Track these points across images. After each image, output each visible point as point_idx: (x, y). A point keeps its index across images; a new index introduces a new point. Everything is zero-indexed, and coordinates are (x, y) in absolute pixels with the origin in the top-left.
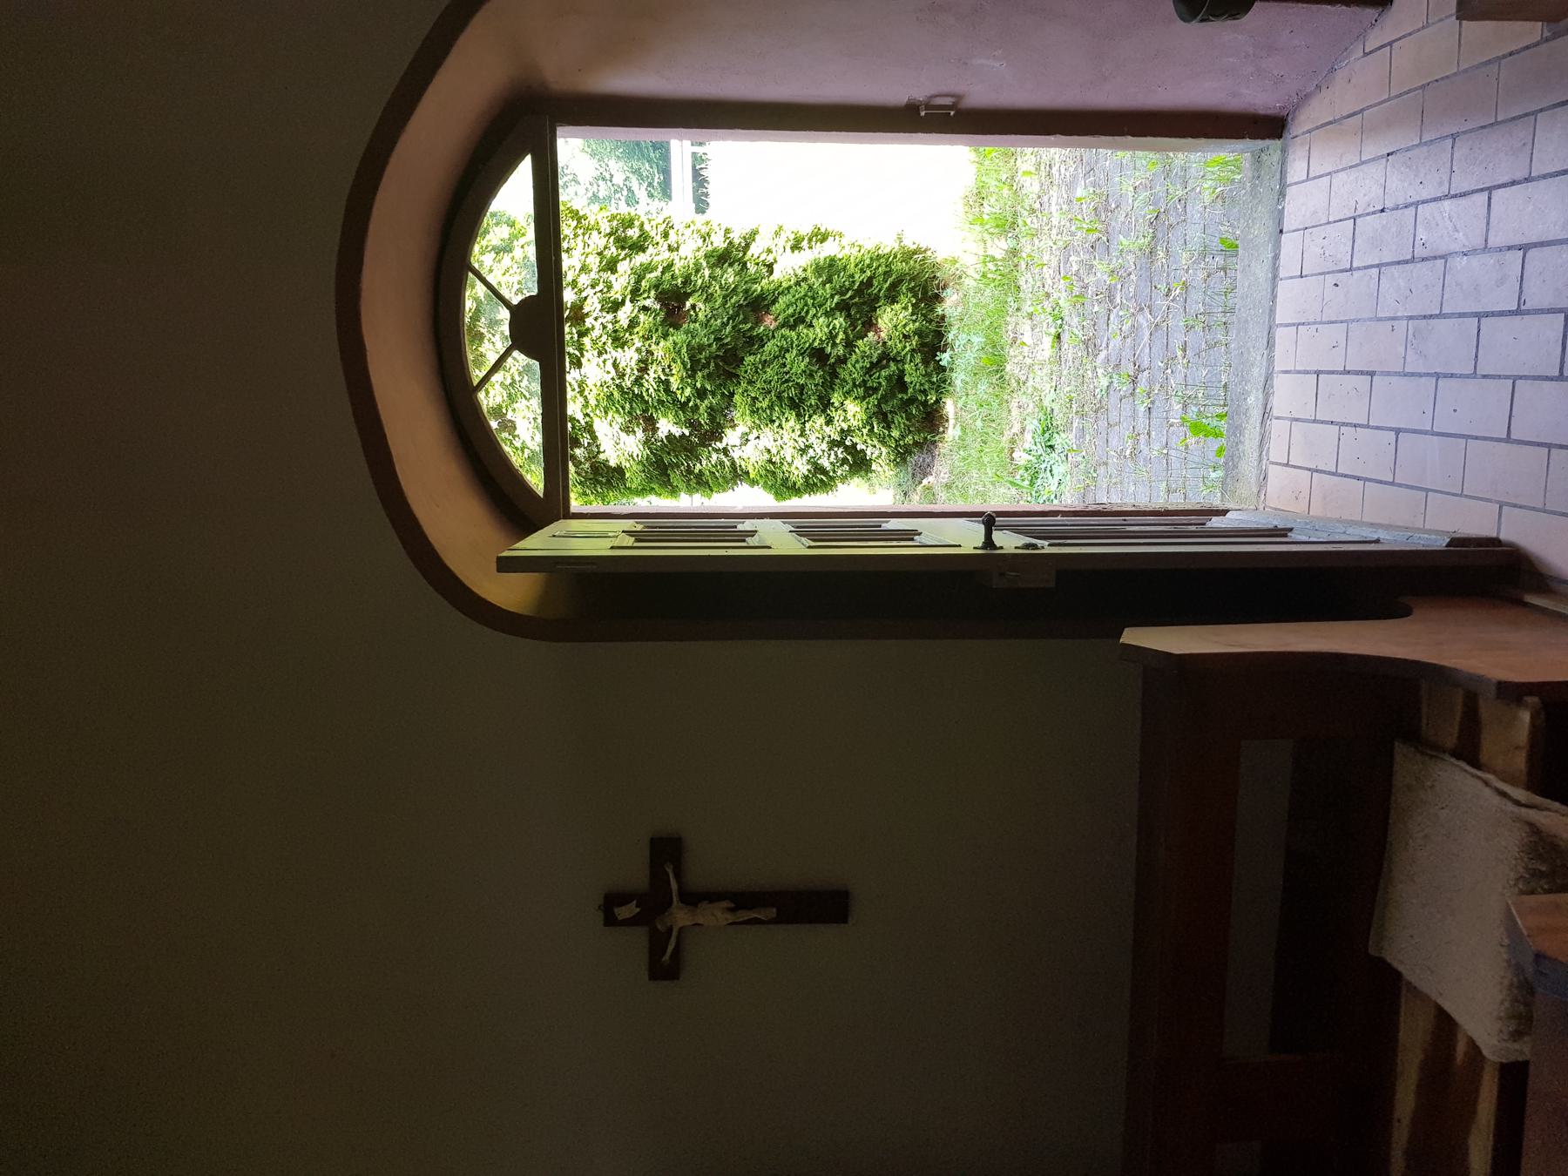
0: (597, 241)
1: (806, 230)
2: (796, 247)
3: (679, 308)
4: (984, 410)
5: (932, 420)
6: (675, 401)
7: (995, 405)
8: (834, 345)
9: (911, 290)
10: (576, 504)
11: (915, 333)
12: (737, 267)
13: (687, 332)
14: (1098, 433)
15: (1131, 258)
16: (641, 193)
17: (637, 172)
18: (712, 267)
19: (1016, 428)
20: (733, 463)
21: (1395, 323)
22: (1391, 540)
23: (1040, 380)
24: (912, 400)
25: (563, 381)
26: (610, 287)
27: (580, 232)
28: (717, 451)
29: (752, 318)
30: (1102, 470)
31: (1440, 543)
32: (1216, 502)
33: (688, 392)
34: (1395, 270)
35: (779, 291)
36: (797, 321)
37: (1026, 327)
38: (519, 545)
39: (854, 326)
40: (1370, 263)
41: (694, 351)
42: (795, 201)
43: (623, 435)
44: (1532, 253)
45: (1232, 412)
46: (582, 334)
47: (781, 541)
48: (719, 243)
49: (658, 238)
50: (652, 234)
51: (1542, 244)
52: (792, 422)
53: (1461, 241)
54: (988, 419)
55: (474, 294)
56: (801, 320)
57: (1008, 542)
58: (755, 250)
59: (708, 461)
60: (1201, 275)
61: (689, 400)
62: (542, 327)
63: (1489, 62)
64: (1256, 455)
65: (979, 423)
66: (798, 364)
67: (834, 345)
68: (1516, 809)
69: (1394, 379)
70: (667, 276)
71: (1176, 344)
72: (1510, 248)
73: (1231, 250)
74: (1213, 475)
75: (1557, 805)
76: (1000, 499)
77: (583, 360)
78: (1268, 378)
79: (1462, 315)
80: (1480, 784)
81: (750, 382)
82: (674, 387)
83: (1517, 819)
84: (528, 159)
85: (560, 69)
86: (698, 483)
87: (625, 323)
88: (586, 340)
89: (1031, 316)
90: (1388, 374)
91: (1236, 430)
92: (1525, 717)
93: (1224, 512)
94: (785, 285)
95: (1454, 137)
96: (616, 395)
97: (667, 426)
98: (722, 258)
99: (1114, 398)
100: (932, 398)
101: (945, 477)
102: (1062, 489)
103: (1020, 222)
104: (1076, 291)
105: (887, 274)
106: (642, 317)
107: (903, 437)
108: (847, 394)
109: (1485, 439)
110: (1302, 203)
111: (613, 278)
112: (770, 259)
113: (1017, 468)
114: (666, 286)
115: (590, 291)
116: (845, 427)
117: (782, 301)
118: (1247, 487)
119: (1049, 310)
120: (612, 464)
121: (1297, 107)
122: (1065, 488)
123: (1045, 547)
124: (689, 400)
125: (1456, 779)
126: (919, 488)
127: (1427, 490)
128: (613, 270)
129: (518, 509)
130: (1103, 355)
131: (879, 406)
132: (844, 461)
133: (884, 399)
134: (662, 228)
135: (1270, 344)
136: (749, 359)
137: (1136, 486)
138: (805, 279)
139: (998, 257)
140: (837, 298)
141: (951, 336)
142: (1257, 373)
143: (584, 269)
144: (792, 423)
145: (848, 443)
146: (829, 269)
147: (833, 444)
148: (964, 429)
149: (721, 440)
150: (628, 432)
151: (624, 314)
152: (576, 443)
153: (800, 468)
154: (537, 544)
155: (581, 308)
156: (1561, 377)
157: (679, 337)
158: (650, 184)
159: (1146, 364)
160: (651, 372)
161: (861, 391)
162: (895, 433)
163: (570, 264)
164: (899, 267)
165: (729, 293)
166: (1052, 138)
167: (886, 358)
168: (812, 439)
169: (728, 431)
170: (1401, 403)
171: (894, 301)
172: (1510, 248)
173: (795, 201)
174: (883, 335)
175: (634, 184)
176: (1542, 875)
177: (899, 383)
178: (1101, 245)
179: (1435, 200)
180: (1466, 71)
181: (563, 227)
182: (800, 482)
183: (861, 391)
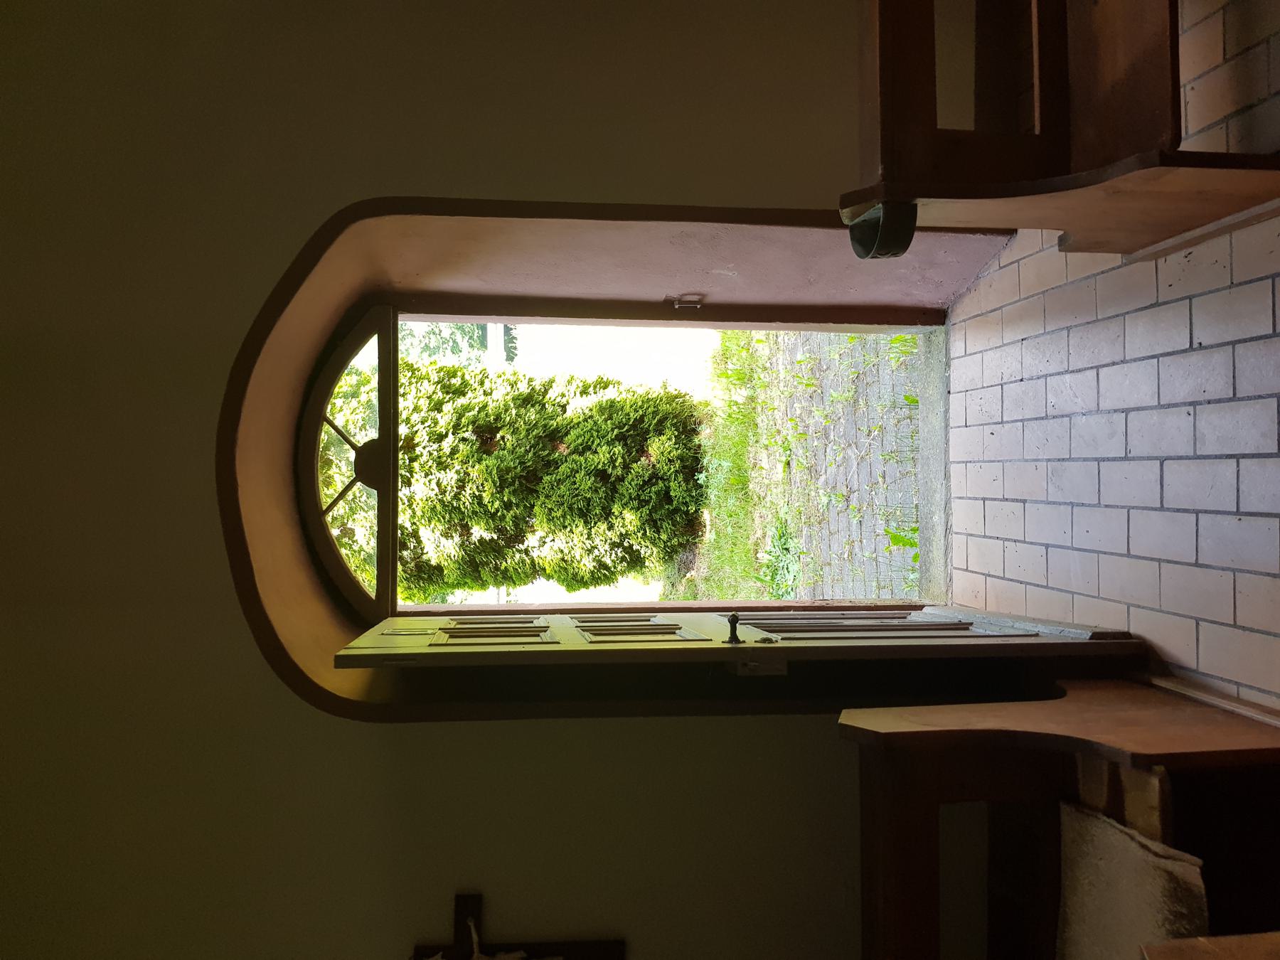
0: (427, 388)
1: (591, 379)
2: (584, 392)
4: (734, 519)
5: (692, 526)
6: (486, 512)
7: (742, 516)
8: (614, 467)
10: (403, 603)
13: (497, 458)
15: (840, 406)
16: (463, 344)
17: (461, 329)
19: (759, 534)
20: (533, 561)
21: (1038, 464)
22: (1049, 634)
23: (776, 496)
24: (676, 510)
25: (396, 497)
26: (436, 424)
27: (414, 380)
28: (519, 551)
30: (827, 569)
31: (1085, 636)
32: (915, 599)
33: (497, 504)
34: (1032, 423)
35: (571, 426)
36: (585, 449)
37: (763, 455)
38: (355, 643)
40: (1016, 418)
41: (503, 473)
42: (582, 364)
43: (443, 540)
44: (1132, 415)
45: (922, 526)
46: (412, 460)
47: (568, 637)
48: (524, 389)
49: (476, 386)
50: (471, 382)
51: (1138, 409)
52: (580, 528)
53: (1079, 405)
54: (737, 526)
55: (326, 434)
56: (589, 448)
57: (750, 636)
58: (552, 394)
59: (512, 560)
60: (893, 422)
62: (380, 465)
63: (1088, 277)
64: (942, 561)
65: (729, 529)
67: (614, 467)
68: (1156, 860)
69: (1040, 506)
70: (482, 414)
71: (878, 472)
72: (1115, 411)
73: (913, 404)
74: (912, 576)
75: (1188, 856)
76: (747, 594)
77: (413, 480)
78: (947, 503)
79: (1085, 460)
80: (1128, 839)
81: (547, 497)
83: (1157, 868)
84: (373, 595)
85: (404, 271)
87: (447, 451)
88: (416, 465)
89: (766, 447)
90: (1036, 502)
91: (927, 541)
92: (1155, 782)
93: (920, 608)
95: (1069, 329)
97: (479, 532)
98: (526, 401)
99: (833, 514)
100: (692, 509)
102: (797, 587)
103: (755, 376)
104: (800, 429)
105: (655, 413)
106: (461, 446)
107: (670, 539)
108: (624, 506)
109: (1112, 554)
110: (962, 373)
111: (439, 416)
112: (564, 401)
113: (761, 567)
114: (481, 422)
115: (420, 426)
116: (623, 531)
117: (573, 433)
118: (938, 587)
119: (780, 443)
120: (433, 563)
121: (955, 303)
122: (798, 583)
123: (779, 641)
124: (497, 511)
125: (1107, 833)
126: (684, 581)
127: (1073, 593)
128: (440, 411)
129: (358, 611)
130: (823, 479)
132: (623, 559)
135: (947, 476)
136: (547, 478)
137: (853, 586)
138: (591, 417)
139: (741, 401)
140: (616, 431)
141: (705, 461)
142: (939, 497)
144: (581, 528)
145: (626, 544)
146: (610, 409)
147: (614, 545)
148: (718, 534)
151: (447, 444)
152: (404, 546)
153: (587, 565)
154: (368, 642)
155: (413, 439)
156: (1275, 334)
157: (490, 461)
158: (471, 338)
159: (855, 487)
160: (467, 489)
161: (636, 503)
162: (664, 537)
163: (404, 405)
164: (664, 407)
165: (531, 427)
167: (655, 477)
168: (597, 541)
169: (529, 535)
172: (1115, 411)
173: (582, 364)
175: (458, 337)
176: (1182, 915)
177: (666, 497)
178: (818, 395)
179: (1059, 374)
180: (1072, 282)
181: (401, 376)
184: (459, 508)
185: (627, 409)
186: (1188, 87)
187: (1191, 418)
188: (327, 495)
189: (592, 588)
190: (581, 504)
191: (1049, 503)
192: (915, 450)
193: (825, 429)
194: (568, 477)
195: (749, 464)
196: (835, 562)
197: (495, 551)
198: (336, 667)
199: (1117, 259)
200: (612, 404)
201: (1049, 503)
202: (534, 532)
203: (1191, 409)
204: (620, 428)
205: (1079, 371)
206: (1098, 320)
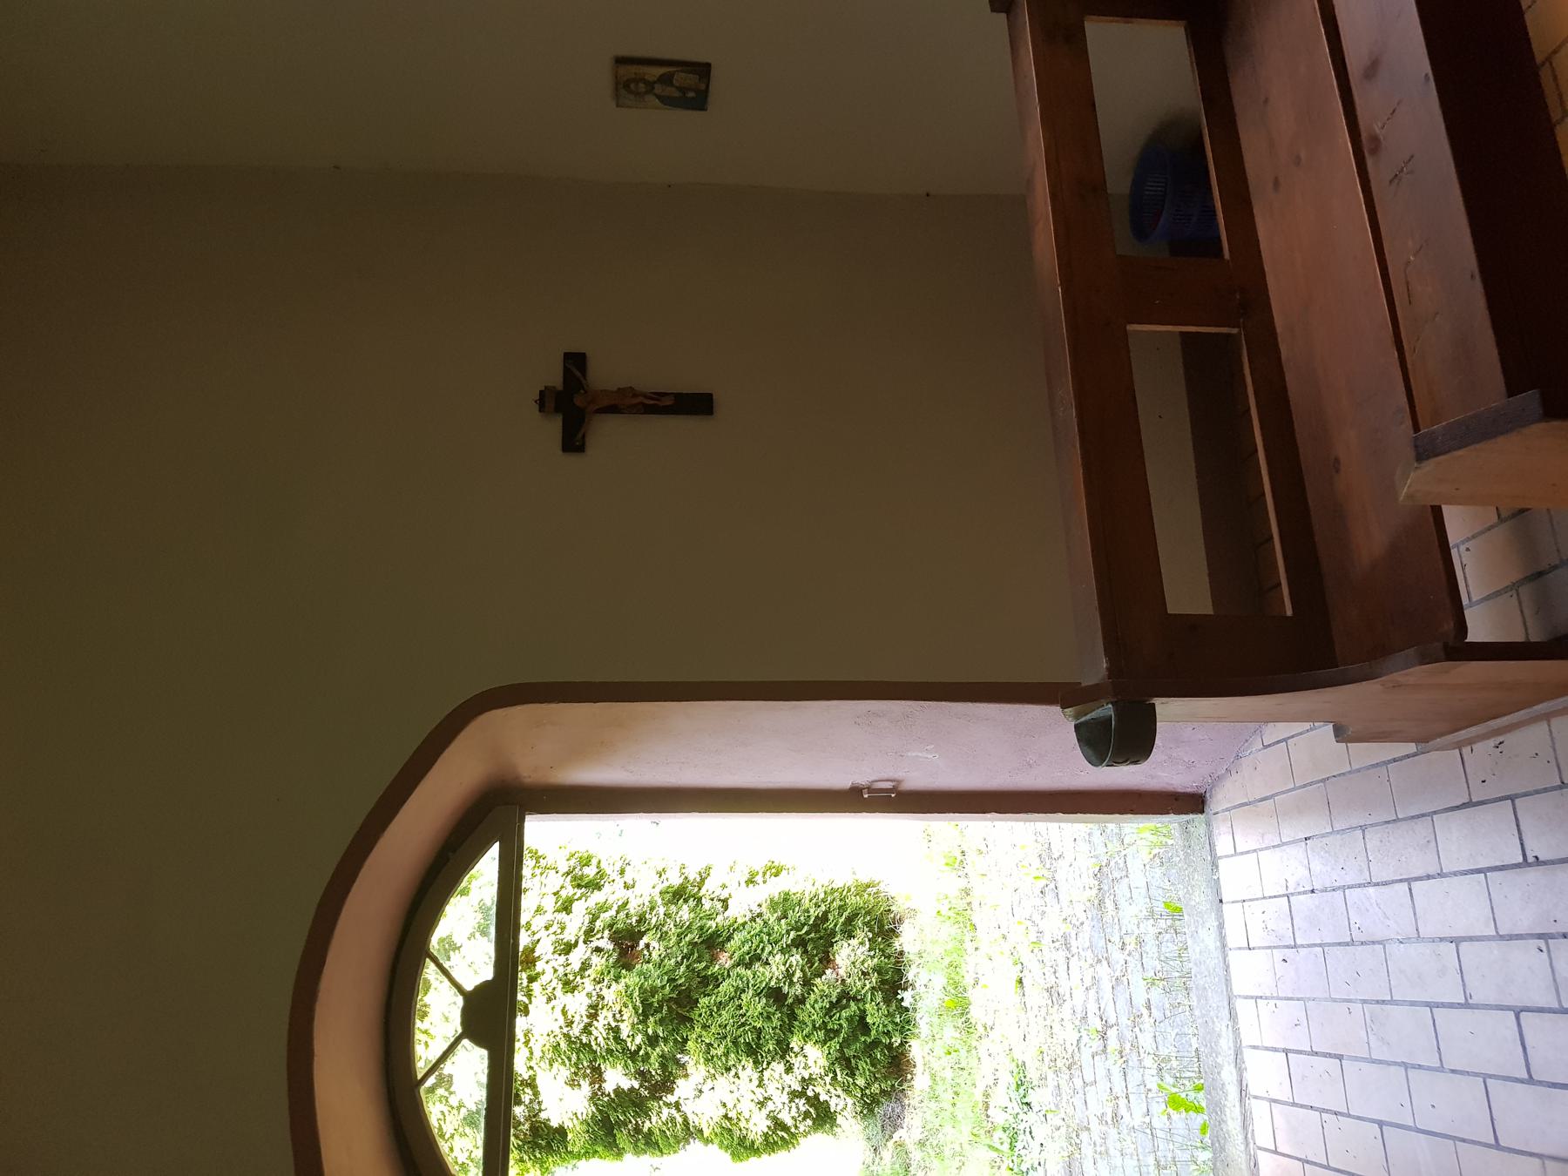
1: (759, 866)
2: (751, 881)
3: (633, 947)
5: (897, 1065)
6: (625, 1050)
7: (963, 1053)
9: (866, 924)
11: (874, 970)
12: (692, 903)
13: (640, 974)
14: (1075, 1092)
18: (665, 904)
24: (876, 1043)
27: (538, 871)
28: (668, 1105)
29: (707, 956)
30: (1084, 1136)
33: (639, 1039)
36: (753, 959)
39: (811, 962)
41: (647, 994)
42: (752, 865)
45: (1207, 1083)
46: (532, 979)
48: (675, 880)
49: (615, 876)
50: (608, 871)
52: (748, 1070)
56: (758, 958)
60: (1153, 931)
61: (639, 1048)
62: (490, 1015)
64: (1241, 1138)
66: (755, 1006)
67: (791, 984)
69: (1363, 1065)
70: (622, 915)
73: (1176, 913)
78: (1238, 1053)
79: (1413, 1003)
81: (705, 1027)
82: (624, 1035)
84: (497, 845)
86: (647, 1144)
87: (576, 966)
88: (536, 986)
90: (1356, 1059)
91: (1217, 1107)
94: (740, 921)
95: (1363, 828)
96: (563, 1046)
97: (617, 1078)
98: (678, 895)
100: (896, 1040)
101: (917, 1134)
105: (842, 908)
107: (868, 1085)
110: (1236, 876)
114: (620, 926)
115: (543, 934)
117: (738, 937)
120: (554, 1124)
121: (1213, 786)
124: (639, 1048)
126: (890, 1144)
130: (1067, 1006)
131: (841, 1051)
132: (807, 1115)
133: (845, 1043)
134: (618, 868)
136: (704, 1001)
138: (760, 915)
140: (793, 934)
142: (1226, 1044)
143: (539, 910)
145: (810, 1093)
146: (784, 904)
147: (794, 1095)
148: (933, 1077)
149: (671, 1091)
150: (572, 1086)
151: (576, 957)
153: (758, 1125)
155: (533, 951)
157: (631, 979)
159: (1112, 1021)
160: (600, 1018)
161: (821, 1034)
163: (528, 903)
164: (853, 901)
166: (988, 815)
167: (845, 997)
169: (680, 1082)
170: (1377, 1094)
171: (851, 936)
172: (1441, 939)
173: (752, 865)
174: (842, 972)
177: (861, 1025)
178: (1050, 888)
179: (1359, 886)
182: (759, 1141)
183: (821, 1034)
184: (590, 1046)
185: (806, 904)
186: (1463, 548)
187: (1545, 955)
188: (425, 1052)
189: (765, 1157)
190: (750, 1037)
191: (1374, 1061)
192: (1187, 976)
193: (1065, 936)
194: (731, 999)
195: (968, 981)
196: (1095, 1125)
197: (635, 1104)
198: (567, 356)
199: (1411, 748)
200: (786, 898)
201: (1374, 1061)
202: (686, 1076)
203: (1542, 943)
204: (798, 930)
205: (1385, 884)
206: (1397, 820)
